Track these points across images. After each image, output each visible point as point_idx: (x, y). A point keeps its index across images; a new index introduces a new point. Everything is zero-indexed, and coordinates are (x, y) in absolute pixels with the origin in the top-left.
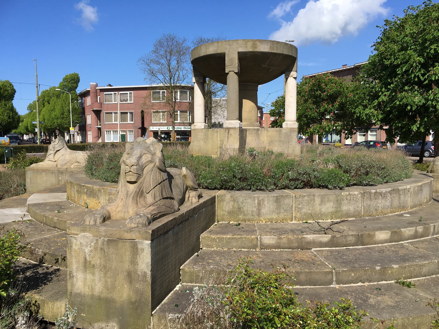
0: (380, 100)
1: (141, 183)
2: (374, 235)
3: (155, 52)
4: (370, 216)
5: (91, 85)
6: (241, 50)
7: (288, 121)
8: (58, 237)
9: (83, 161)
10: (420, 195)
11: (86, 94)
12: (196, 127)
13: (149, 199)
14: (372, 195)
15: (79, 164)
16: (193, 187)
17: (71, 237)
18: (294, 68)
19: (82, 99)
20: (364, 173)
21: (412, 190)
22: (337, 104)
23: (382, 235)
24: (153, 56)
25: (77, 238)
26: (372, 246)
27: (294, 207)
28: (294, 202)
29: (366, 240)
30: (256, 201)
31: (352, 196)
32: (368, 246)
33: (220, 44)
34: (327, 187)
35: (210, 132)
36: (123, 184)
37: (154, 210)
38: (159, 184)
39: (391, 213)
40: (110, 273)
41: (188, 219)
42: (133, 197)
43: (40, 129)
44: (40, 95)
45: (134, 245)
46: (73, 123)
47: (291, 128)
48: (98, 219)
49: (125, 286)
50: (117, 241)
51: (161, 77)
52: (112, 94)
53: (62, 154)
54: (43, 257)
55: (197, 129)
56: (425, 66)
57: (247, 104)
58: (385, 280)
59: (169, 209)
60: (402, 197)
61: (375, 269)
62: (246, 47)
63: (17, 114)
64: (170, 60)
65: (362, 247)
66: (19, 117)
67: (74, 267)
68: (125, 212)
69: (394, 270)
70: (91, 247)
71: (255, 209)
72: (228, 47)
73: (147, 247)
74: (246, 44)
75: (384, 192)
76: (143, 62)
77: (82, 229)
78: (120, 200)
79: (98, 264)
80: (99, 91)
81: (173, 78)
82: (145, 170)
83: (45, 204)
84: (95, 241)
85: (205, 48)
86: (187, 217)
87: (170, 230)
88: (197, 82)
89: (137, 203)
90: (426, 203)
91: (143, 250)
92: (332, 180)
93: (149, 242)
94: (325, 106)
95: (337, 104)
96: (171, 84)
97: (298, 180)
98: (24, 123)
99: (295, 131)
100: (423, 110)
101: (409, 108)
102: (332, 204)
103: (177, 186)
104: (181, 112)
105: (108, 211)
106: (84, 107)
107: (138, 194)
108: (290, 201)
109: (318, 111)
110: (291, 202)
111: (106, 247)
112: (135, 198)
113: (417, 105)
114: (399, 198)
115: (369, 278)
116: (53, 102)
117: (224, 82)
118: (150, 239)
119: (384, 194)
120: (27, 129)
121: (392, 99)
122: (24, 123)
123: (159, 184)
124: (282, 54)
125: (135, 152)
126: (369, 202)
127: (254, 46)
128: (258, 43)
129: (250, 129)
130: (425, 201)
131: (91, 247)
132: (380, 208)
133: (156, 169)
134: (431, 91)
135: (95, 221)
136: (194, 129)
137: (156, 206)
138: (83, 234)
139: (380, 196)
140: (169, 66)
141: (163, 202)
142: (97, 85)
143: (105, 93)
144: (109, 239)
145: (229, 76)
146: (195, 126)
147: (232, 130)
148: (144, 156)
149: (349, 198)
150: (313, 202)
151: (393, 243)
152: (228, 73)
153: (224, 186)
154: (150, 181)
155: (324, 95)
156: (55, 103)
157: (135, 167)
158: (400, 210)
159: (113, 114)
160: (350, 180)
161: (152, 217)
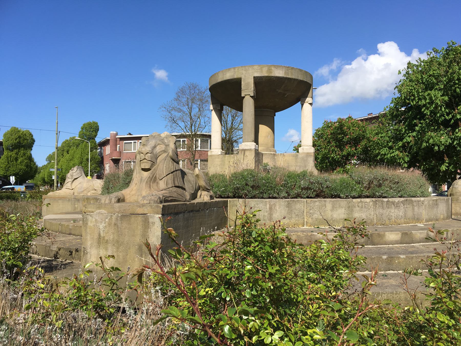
0: (405, 140)
1: (154, 170)
2: (384, 235)
3: (176, 100)
4: (383, 225)
6: (257, 75)
8: (73, 240)
9: (100, 189)
10: (435, 209)
11: (105, 143)
12: (213, 153)
13: (162, 184)
14: (385, 204)
15: (96, 192)
16: (205, 187)
17: (88, 214)
18: (310, 94)
19: (101, 149)
20: (376, 185)
21: (426, 203)
22: (360, 148)
23: (392, 236)
24: (175, 104)
25: (93, 216)
26: (382, 246)
27: (305, 212)
28: (305, 207)
29: (376, 240)
30: (268, 206)
31: (364, 204)
33: (236, 69)
34: (340, 197)
35: (226, 158)
36: (138, 171)
37: (166, 193)
38: (172, 173)
39: (405, 224)
41: (198, 211)
42: (147, 182)
43: (58, 177)
44: (60, 145)
45: (145, 219)
46: (90, 172)
47: (308, 153)
48: (113, 199)
49: (136, 259)
51: (182, 124)
52: (131, 143)
53: (79, 182)
54: (57, 252)
56: (451, 105)
57: (264, 129)
58: (392, 270)
59: (180, 197)
60: (416, 208)
61: (381, 257)
62: (262, 72)
63: (35, 164)
66: (37, 167)
67: (89, 243)
68: (138, 196)
69: (400, 260)
70: (105, 223)
71: (266, 214)
72: (244, 72)
74: (261, 69)
75: (397, 201)
76: (164, 109)
77: (98, 206)
78: (134, 185)
79: (111, 239)
80: (118, 140)
83: (63, 219)
84: (109, 217)
85: (222, 74)
86: (198, 208)
87: (180, 213)
88: (215, 109)
89: (150, 187)
90: (443, 219)
91: (154, 223)
92: (344, 190)
93: (160, 216)
94: (348, 149)
95: (360, 148)
96: (192, 132)
97: (310, 189)
98: (41, 175)
100: (450, 150)
101: (436, 148)
102: (343, 210)
103: (189, 181)
104: (201, 161)
105: (123, 194)
107: (151, 179)
110: (303, 207)
111: (119, 223)
112: (149, 183)
113: (443, 144)
114: (413, 209)
116: (73, 151)
117: (240, 108)
118: (161, 213)
119: (397, 204)
120: (44, 180)
121: (419, 141)
122: (41, 175)
123: (172, 173)
124: (297, 80)
125: (151, 142)
126: (381, 211)
127: (269, 70)
128: (273, 68)
129: (266, 154)
130: (442, 217)
131: (105, 223)
133: (170, 159)
134: (457, 130)
135: (111, 200)
136: (211, 156)
138: (98, 211)
139: (393, 206)
141: (175, 189)
142: (117, 134)
143: (125, 142)
145: (244, 100)
146: (211, 152)
147: (248, 151)
148: (158, 147)
149: (360, 205)
151: (404, 245)
152: (244, 97)
153: (237, 195)
156: (74, 152)
157: (149, 154)
158: (414, 221)
159: (132, 163)
160: (363, 191)
161: (164, 198)
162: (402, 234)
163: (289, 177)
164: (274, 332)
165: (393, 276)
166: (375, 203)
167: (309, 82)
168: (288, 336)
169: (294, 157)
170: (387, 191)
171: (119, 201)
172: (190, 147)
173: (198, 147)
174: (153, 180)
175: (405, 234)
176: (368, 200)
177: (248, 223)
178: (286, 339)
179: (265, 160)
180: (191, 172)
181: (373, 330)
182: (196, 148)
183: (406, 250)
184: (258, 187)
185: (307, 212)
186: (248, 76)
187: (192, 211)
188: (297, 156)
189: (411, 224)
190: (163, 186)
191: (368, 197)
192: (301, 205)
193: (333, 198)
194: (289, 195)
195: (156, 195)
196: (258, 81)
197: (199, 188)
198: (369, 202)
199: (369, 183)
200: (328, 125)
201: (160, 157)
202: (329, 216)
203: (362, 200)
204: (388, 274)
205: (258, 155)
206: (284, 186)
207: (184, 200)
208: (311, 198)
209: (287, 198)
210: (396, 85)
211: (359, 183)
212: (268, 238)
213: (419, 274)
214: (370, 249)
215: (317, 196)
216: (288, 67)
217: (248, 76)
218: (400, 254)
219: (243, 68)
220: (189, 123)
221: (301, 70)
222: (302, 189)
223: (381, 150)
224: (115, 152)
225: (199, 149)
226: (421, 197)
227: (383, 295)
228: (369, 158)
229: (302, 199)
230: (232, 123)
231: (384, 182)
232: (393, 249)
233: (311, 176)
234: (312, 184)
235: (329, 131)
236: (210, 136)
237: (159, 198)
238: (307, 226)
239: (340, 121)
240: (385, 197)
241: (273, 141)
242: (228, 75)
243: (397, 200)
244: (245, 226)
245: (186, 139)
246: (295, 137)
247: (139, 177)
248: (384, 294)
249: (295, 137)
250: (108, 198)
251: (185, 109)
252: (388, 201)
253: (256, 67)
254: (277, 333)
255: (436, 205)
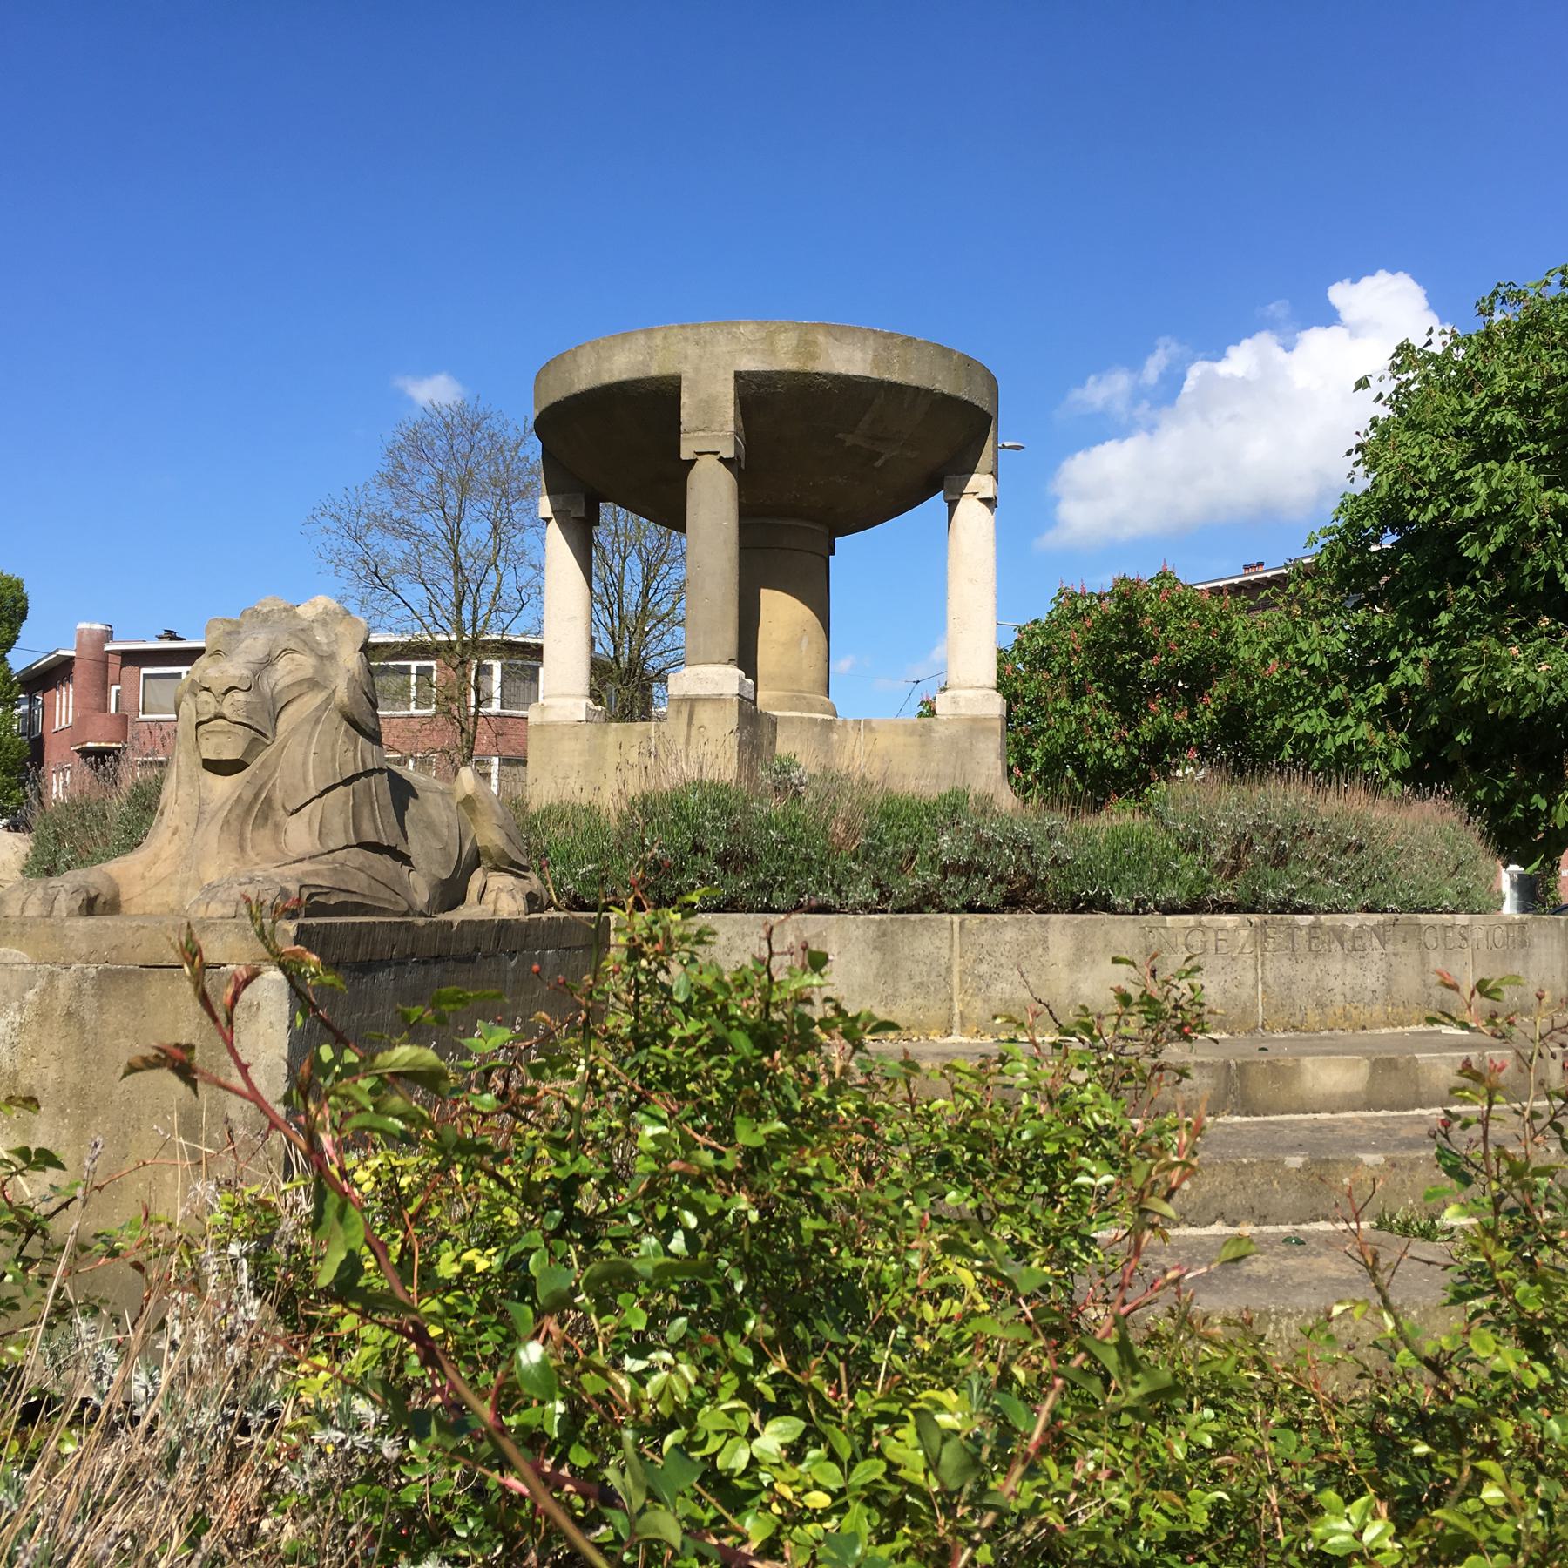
0: (1396, 679)
2: (1294, 1072)
5: (81, 632)
6: (751, 363)
7: (960, 688)
11: (54, 674)
12: (551, 716)
13: (299, 834)
18: (986, 459)
19: (32, 700)
20: (1266, 858)
21: (1479, 935)
23: (1330, 1075)
24: (384, 500)
27: (956, 969)
28: (956, 947)
29: (1262, 1090)
31: (1211, 934)
32: (1272, 1118)
33: (658, 339)
34: (1109, 908)
37: (317, 874)
39: (1387, 1025)
40: (104, 1122)
41: (470, 959)
42: (227, 821)
47: (975, 720)
48: (62, 896)
50: (141, 975)
51: (415, 594)
55: (552, 725)
57: (781, 611)
58: (1326, 1218)
59: (387, 894)
61: (1280, 1163)
62: (773, 352)
64: (459, 519)
65: (1246, 1119)
68: (184, 885)
69: (1365, 1176)
70: (21, 1009)
72: (692, 351)
73: (271, 994)
74: (770, 339)
75: (1352, 926)
76: (333, 526)
78: (169, 833)
80: (115, 661)
81: (469, 598)
82: (283, 717)
84: (41, 983)
86: (467, 947)
87: (384, 964)
88: (560, 515)
89: (242, 848)
94: (1160, 717)
95: (1209, 708)
96: (461, 632)
97: (981, 870)
99: (985, 731)
103: (430, 826)
105: (110, 879)
106: (41, 739)
107: (248, 811)
108: (938, 943)
109: (1129, 736)
110: (945, 952)
111: (90, 1002)
112: (235, 825)
114: (1424, 962)
115: (1256, 1204)
117: (673, 515)
119: (1354, 939)
121: (1443, 675)
124: (929, 392)
125: (249, 642)
126: (1286, 967)
127: (806, 348)
128: (821, 339)
129: (791, 719)
131: (21, 1009)
132: (1339, 998)
133: (337, 717)
135: (50, 903)
137: (327, 863)
139: (1336, 945)
140: (454, 544)
141: (358, 857)
142: (108, 636)
144: (107, 970)
145: (694, 477)
148: (282, 662)
150: (1040, 950)
151: (1382, 1113)
152: (692, 463)
154: (305, 764)
155: (1148, 670)
160: (1209, 880)
161: (306, 893)
162: (1375, 1065)
163: (886, 816)
164: (764, 1420)
165: (1328, 1242)
166: (1260, 932)
167: (984, 405)
168: (824, 1438)
169: (912, 734)
170: (1311, 881)
171: (90, 906)
172: (449, 703)
173: (489, 698)
174: (259, 811)
175: (1384, 1066)
176: (1230, 920)
177: (652, 939)
178: (813, 1454)
179: (785, 745)
180: (440, 786)
181: (1210, 1433)
182: (479, 703)
183: (1390, 1133)
184: (750, 858)
185: (963, 972)
186: (710, 369)
187: (438, 958)
188: (929, 730)
189: (1414, 1028)
190: (304, 845)
191: (1231, 909)
192: (939, 938)
193: (1081, 911)
194: (884, 897)
195: (268, 879)
196: (755, 394)
197: (475, 859)
198: (1236, 929)
199: (1236, 849)
200: (1071, 608)
201: (290, 710)
202: (1063, 989)
203: (1205, 918)
204: (1309, 1235)
205: (753, 724)
206: (866, 855)
207: (404, 906)
208: (984, 909)
209: (876, 911)
210: (1359, 440)
211: (1194, 848)
212: (743, 1007)
213: (1443, 1232)
214: (1235, 1130)
215: (1012, 903)
216: (891, 335)
217: (710, 369)
218: (1365, 1148)
219: (689, 333)
220: (448, 588)
221: (946, 352)
222: (945, 871)
223: (1297, 719)
224: (100, 719)
225: (495, 707)
226: (1456, 911)
227: (1285, 1321)
228: (1242, 744)
229: (946, 917)
230: (645, 594)
231: (1300, 845)
232: (1332, 1129)
233: (984, 812)
234: (988, 849)
235: (1074, 637)
236: (537, 652)
237: (284, 893)
238: (963, 1030)
239: (1126, 594)
240: (1304, 910)
241: (821, 664)
242: (622, 363)
243: (1353, 921)
244: (644, 955)
245: (433, 663)
246: (927, 647)
247: (191, 796)
248: (1290, 1315)
249: (927, 647)
250: (40, 892)
251: (431, 523)
252: (1313, 927)
253: (746, 330)
254: (775, 1425)
255: (1523, 944)
